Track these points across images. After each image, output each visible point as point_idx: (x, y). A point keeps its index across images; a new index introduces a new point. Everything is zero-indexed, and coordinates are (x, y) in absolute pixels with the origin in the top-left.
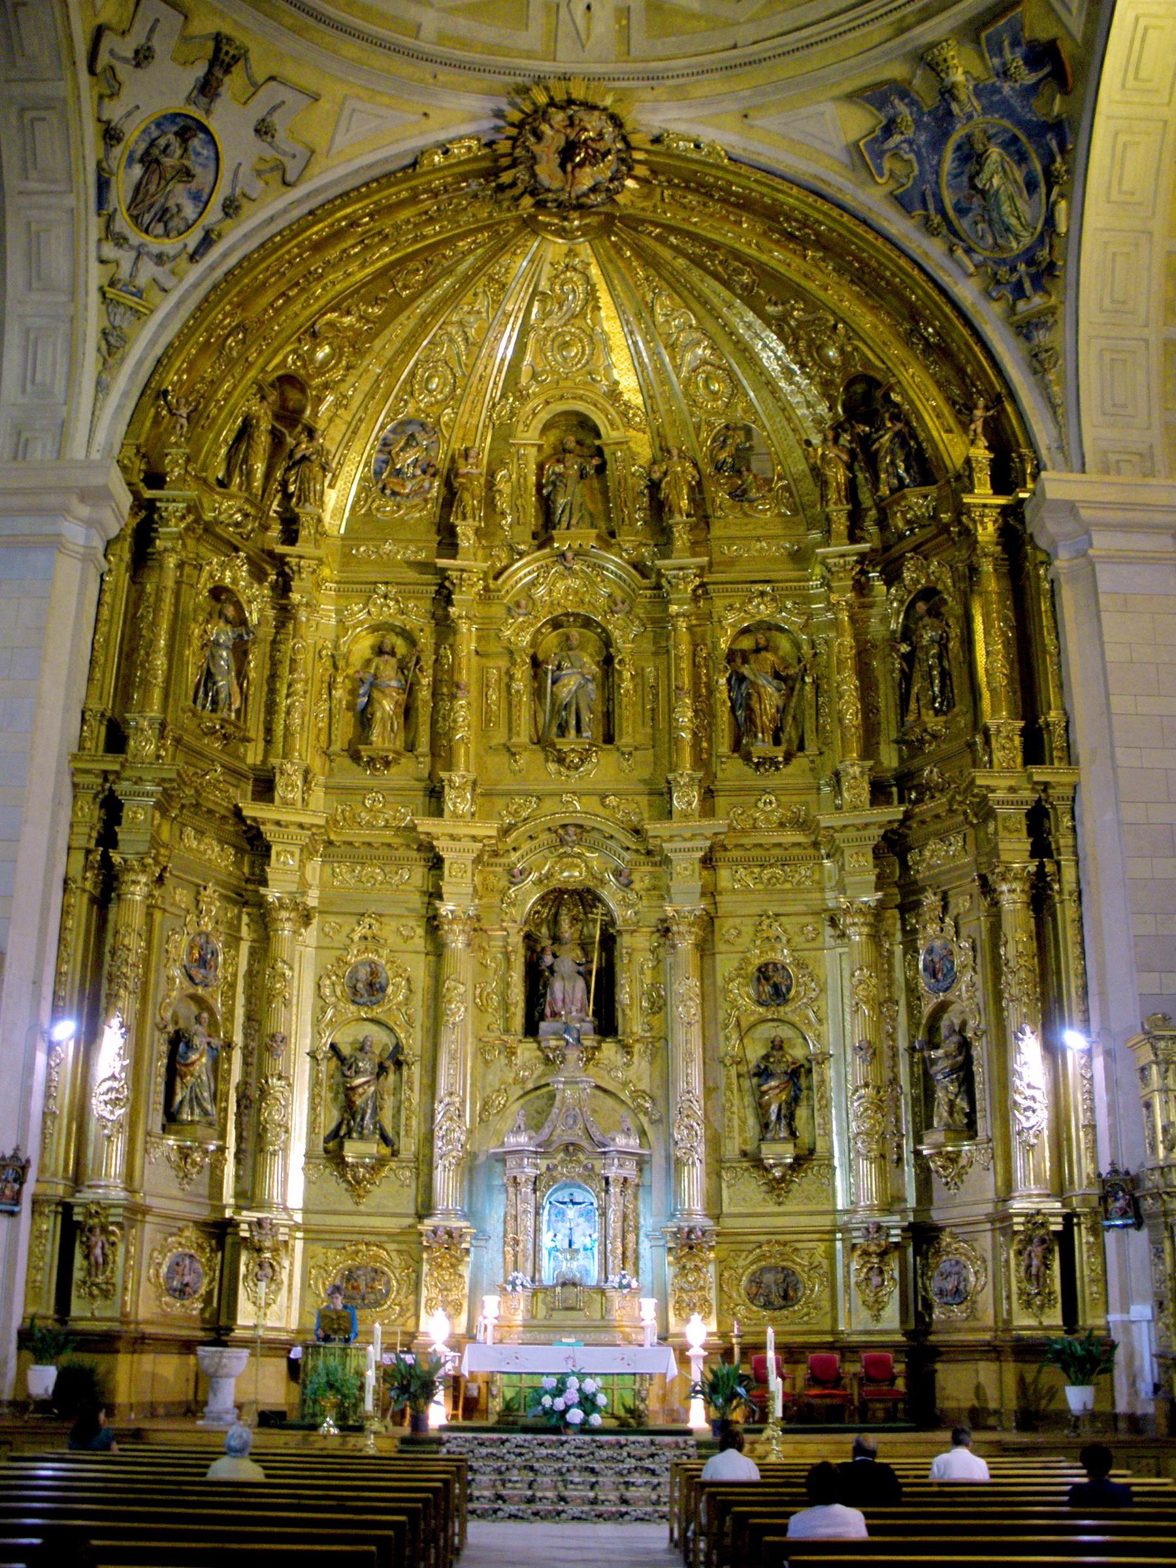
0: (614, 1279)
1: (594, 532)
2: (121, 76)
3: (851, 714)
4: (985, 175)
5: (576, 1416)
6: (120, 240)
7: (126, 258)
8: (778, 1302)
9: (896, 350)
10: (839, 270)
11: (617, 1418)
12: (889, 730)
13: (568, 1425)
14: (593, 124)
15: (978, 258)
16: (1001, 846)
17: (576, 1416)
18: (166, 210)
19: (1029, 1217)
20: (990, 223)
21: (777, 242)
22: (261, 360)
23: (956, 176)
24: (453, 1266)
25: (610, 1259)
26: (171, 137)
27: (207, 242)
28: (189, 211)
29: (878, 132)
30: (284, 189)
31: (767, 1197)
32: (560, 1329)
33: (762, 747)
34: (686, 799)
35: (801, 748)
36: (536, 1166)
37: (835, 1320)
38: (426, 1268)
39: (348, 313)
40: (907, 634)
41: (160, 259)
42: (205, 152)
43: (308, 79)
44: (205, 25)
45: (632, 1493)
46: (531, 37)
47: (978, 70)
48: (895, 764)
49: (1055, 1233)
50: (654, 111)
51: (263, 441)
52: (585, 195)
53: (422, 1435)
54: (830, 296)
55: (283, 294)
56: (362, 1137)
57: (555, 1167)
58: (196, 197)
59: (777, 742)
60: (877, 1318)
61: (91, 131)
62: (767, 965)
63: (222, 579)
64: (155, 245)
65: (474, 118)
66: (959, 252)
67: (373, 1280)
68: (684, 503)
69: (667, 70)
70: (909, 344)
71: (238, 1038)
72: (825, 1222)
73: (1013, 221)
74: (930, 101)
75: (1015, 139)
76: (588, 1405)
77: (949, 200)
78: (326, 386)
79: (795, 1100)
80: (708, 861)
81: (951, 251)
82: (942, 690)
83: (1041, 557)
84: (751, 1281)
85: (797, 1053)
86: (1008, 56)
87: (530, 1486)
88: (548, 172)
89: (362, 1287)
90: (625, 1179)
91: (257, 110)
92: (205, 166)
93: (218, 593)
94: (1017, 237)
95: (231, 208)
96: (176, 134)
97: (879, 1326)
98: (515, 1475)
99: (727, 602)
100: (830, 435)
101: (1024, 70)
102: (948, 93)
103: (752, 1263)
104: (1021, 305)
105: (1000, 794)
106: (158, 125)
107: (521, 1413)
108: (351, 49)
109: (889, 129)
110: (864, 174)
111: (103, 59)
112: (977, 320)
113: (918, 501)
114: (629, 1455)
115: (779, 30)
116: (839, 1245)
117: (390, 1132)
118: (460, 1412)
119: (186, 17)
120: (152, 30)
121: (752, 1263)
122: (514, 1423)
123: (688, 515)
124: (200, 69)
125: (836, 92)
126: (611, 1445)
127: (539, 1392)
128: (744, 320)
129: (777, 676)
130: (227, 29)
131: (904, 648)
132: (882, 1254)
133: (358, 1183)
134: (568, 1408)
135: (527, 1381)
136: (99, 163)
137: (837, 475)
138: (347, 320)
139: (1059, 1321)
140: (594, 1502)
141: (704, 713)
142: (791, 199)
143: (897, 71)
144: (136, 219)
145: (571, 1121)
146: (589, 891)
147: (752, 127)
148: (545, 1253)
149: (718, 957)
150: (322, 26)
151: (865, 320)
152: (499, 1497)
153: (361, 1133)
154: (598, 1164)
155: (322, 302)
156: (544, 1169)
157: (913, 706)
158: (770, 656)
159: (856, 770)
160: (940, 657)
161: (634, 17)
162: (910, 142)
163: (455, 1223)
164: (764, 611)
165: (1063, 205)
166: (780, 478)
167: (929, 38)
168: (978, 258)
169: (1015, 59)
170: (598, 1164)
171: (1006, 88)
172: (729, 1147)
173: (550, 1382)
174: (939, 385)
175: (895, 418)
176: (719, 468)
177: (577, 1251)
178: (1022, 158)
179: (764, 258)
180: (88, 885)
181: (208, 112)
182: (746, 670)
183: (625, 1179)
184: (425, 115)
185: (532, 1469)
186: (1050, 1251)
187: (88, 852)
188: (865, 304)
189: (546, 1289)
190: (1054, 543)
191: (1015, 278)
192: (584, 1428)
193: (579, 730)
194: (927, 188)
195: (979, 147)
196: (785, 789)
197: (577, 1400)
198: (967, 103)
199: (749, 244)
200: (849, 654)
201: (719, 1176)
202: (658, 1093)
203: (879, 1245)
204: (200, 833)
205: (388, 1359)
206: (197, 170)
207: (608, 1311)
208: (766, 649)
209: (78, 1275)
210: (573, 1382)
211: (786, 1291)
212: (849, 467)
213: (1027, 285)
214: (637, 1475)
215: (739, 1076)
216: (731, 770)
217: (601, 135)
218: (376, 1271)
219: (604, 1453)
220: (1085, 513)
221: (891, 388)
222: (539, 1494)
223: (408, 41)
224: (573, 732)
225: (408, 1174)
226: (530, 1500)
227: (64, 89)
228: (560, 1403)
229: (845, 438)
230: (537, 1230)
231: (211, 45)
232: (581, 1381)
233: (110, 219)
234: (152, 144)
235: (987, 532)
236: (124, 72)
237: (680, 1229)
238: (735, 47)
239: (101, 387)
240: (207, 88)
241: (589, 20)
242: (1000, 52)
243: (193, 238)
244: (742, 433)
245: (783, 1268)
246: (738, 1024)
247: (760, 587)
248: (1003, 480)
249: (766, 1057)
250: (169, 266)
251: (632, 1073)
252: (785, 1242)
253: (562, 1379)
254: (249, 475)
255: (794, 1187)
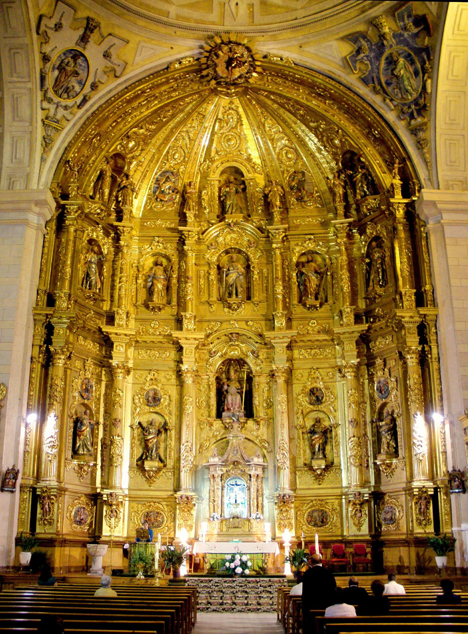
0: (254, 515)
1: (242, 215)
2: (49, 35)
3: (346, 288)
4: (397, 70)
5: (239, 570)
6: (50, 101)
7: (52, 108)
8: (320, 524)
9: (363, 140)
10: (339, 108)
11: (256, 571)
12: (361, 294)
13: (236, 574)
14: (240, 51)
15: (395, 103)
16: (407, 340)
17: (239, 570)
18: (68, 88)
19: (420, 489)
20: (400, 89)
21: (314, 97)
22: (107, 148)
23: (386, 70)
24: (188, 511)
25: (252, 507)
26: (70, 59)
27: (85, 101)
28: (77, 88)
29: (354, 53)
30: (115, 79)
31: (315, 482)
32: (232, 535)
33: (310, 301)
34: (280, 322)
35: (326, 301)
36: (222, 470)
37: (342, 531)
38: (178, 511)
39: (142, 128)
40: (368, 255)
41: (66, 108)
42: (83, 65)
43: (125, 34)
44: (83, 14)
45: (262, 601)
46: (214, 16)
47: (394, 27)
48: (364, 307)
49: (431, 495)
50: (264, 45)
51: (108, 180)
52: (236, 79)
53: (178, 579)
54: (336, 119)
55: (115, 121)
56: (152, 459)
57: (230, 471)
58: (80, 83)
59: (316, 299)
60: (359, 530)
61: (38, 58)
62: (313, 388)
63: (92, 236)
64: (64, 102)
65: (192, 49)
66: (388, 101)
67: (157, 517)
68: (278, 203)
69: (270, 29)
70: (367, 137)
71: (101, 421)
72: (338, 491)
73: (409, 88)
74: (375, 40)
75: (409, 55)
76: (244, 566)
77: (383, 80)
78: (133, 158)
79: (325, 443)
80: (289, 347)
81: (384, 100)
82: (383, 277)
83: (422, 223)
84: (308, 516)
85: (326, 424)
86: (406, 21)
87: (221, 598)
88: (221, 70)
89: (152, 519)
90: (258, 475)
91: (104, 47)
92: (83, 70)
93: (91, 241)
94: (411, 94)
95: (94, 87)
96: (72, 57)
97: (360, 533)
98: (215, 594)
99: (296, 242)
100: (337, 175)
101: (413, 27)
102: (382, 36)
103: (309, 508)
104: (413, 122)
105: (407, 319)
106: (64, 54)
107: (217, 569)
108: (141, 22)
109: (359, 51)
110: (348, 70)
111: (43, 28)
112: (395, 128)
113: (372, 201)
114: (261, 586)
115: (314, 12)
116: (344, 500)
117: (163, 458)
118: (192, 569)
119: (75, 11)
120: (62, 16)
121: (309, 508)
122: (214, 573)
123: (280, 208)
124: (81, 32)
125: (337, 37)
126: (253, 582)
127: (224, 561)
128: (301, 129)
129: (316, 272)
130: (92, 15)
131: (367, 260)
132: (361, 504)
133: (150, 478)
134: (236, 567)
135: (219, 557)
136: (41, 70)
137: (340, 191)
138: (141, 131)
139: (433, 531)
140: (247, 604)
141: (287, 287)
142: (319, 80)
143: (361, 28)
144: (56, 92)
145: (235, 452)
146: (241, 359)
147: (303, 51)
148: (225, 506)
149: (294, 386)
150: (130, 14)
151: (351, 129)
152: (209, 603)
153: (151, 458)
154: (247, 469)
155: (131, 124)
156: (225, 472)
157: (371, 284)
158: (313, 264)
159: (349, 310)
160: (382, 264)
161: (255, 7)
162: (367, 56)
163: (189, 494)
164: (311, 246)
165: (429, 81)
166: (317, 192)
167: (374, 15)
168: (395, 103)
169: (410, 23)
170: (247, 469)
171: (406, 34)
172: (299, 462)
173: (229, 557)
174: (381, 155)
175: (362, 168)
176: (292, 189)
177: (238, 504)
178: (412, 63)
179: (309, 104)
180: (41, 360)
181: (84, 48)
182: (304, 270)
183: (258, 475)
184: (172, 48)
185: (222, 591)
186: (429, 502)
187: (40, 346)
188: (350, 122)
189: (226, 520)
190: (427, 218)
191: (410, 111)
192: (243, 575)
193: (237, 295)
194: (375, 75)
195: (395, 58)
196: (320, 318)
197: (239, 564)
198: (390, 40)
199: (303, 98)
200: (345, 263)
201: (295, 474)
202: (271, 440)
203: (360, 501)
204: (85, 338)
205: (164, 548)
206: (80, 72)
207: (251, 528)
208: (312, 261)
209: (39, 516)
210: (238, 557)
211: (323, 520)
212: (344, 188)
213: (415, 114)
214: (264, 593)
215: (303, 433)
216: (298, 310)
217: (242, 55)
218: (158, 513)
219: (250, 585)
220: (439, 206)
221: (361, 156)
222: (225, 602)
223: (165, 19)
224: (234, 296)
225: (170, 474)
226: (222, 604)
227: (27, 40)
228: (232, 565)
229: (343, 176)
230: (222, 496)
231: (85, 22)
232: (241, 556)
233: (46, 92)
234: (62, 62)
235: (400, 213)
236: (50, 33)
237: (280, 495)
238: (296, 19)
239: (43, 160)
240: (84, 39)
241: (237, 9)
242: (403, 20)
243: (79, 99)
244: (301, 174)
245: (322, 510)
246: (302, 413)
247: (309, 236)
248: (406, 193)
249: (313, 426)
250: (69, 111)
251: (260, 432)
252: (322, 500)
253: (233, 556)
254: (103, 194)
255: (325, 477)
